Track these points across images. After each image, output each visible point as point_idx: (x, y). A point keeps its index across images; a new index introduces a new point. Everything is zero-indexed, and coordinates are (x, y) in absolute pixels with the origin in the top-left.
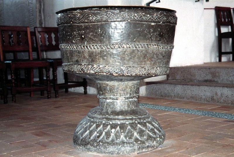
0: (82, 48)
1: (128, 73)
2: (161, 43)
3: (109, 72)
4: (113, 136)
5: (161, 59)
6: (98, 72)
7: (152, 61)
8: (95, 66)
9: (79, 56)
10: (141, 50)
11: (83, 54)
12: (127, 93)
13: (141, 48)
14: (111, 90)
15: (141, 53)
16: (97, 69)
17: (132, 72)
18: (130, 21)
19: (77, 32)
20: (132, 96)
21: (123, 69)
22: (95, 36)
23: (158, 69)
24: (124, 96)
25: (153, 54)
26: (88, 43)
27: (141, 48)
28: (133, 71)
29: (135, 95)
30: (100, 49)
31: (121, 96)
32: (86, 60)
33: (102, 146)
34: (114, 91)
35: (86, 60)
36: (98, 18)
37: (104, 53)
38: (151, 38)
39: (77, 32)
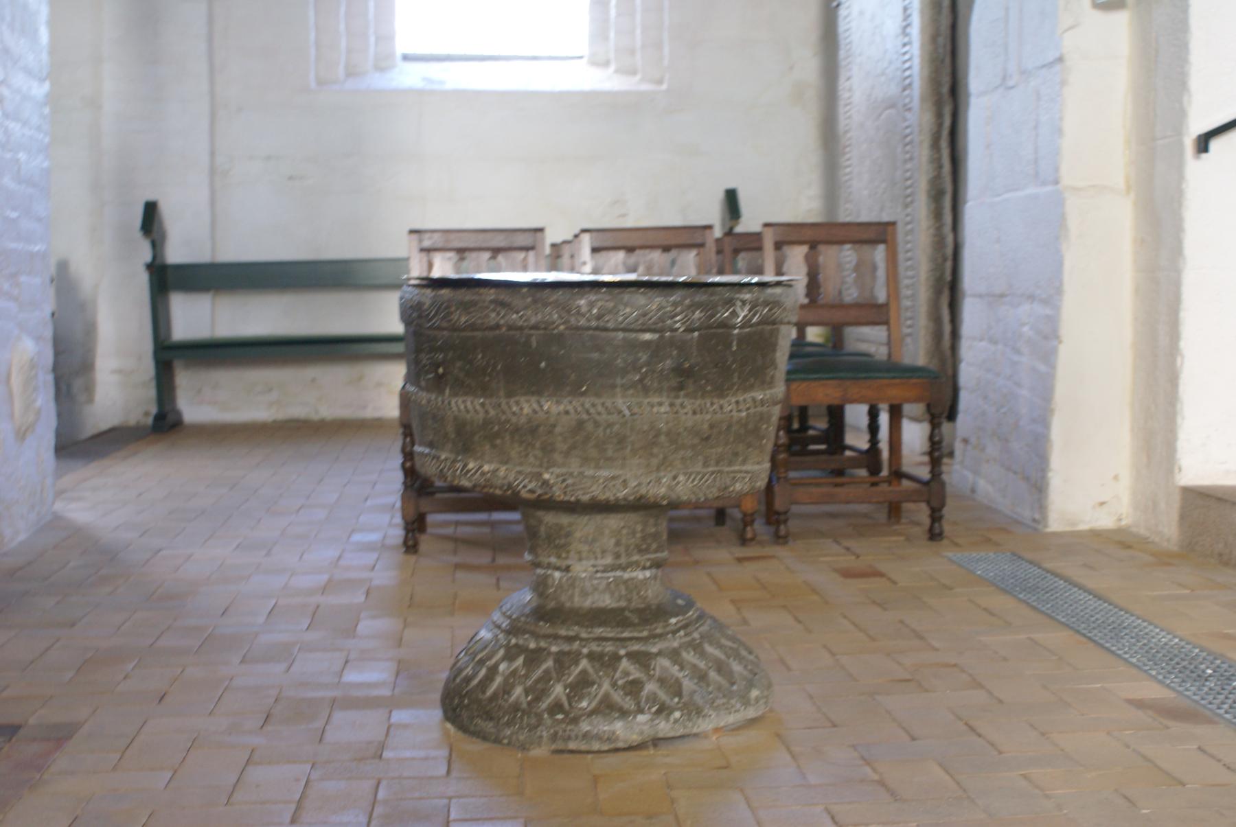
2: (686, 396)
8: (471, 466)
14: (549, 538)
20: (623, 560)
31: (580, 559)
32: (450, 445)
38: (641, 380)
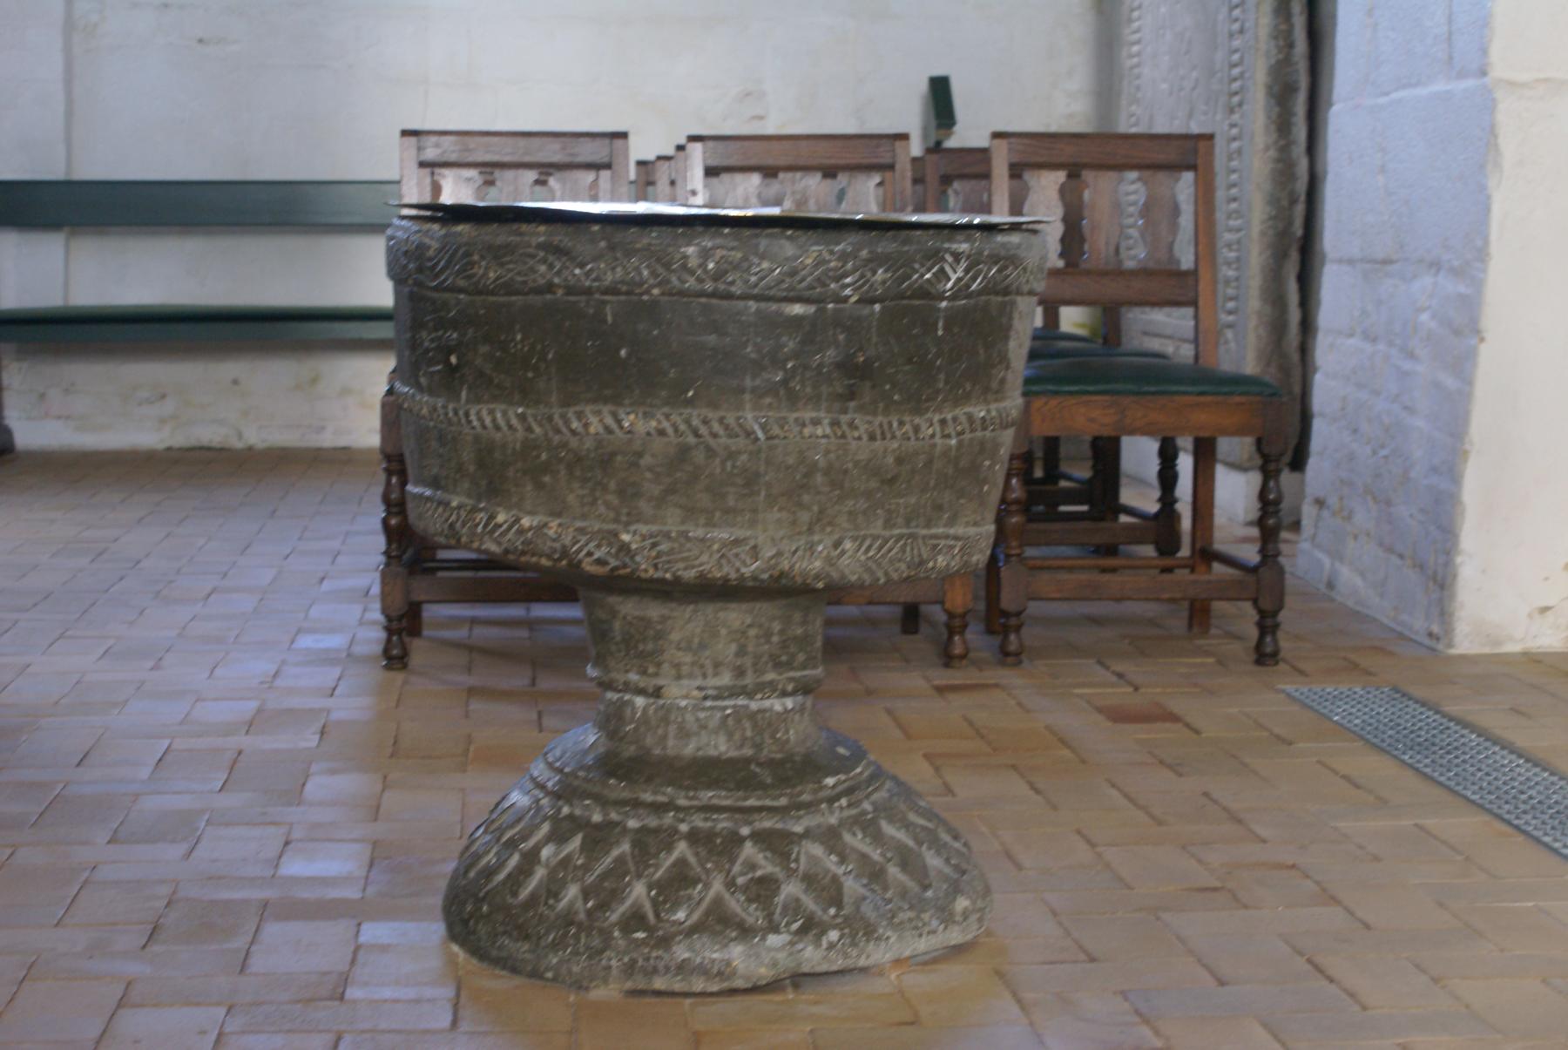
1: (656, 567)
3: (565, 552)
5: (868, 494)
7: (800, 505)
10: (727, 448)
12: (717, 665)
13: (723, 440)
15: (729, 464)
16: (510, 535)
17: (681, 565)
18: (663, 294)
20: (749, 680)
21: (634, 546)
23: (843, 552)
24: (699, 682)
25: (803, 469)
27: (723, 440)
28: (683, 559)
29: (770, 676)
30: (520, 434)
31: (679, 677)
34: (641, 647)
36: (510, 271)
37: (538, 456)
38: (785, 382)
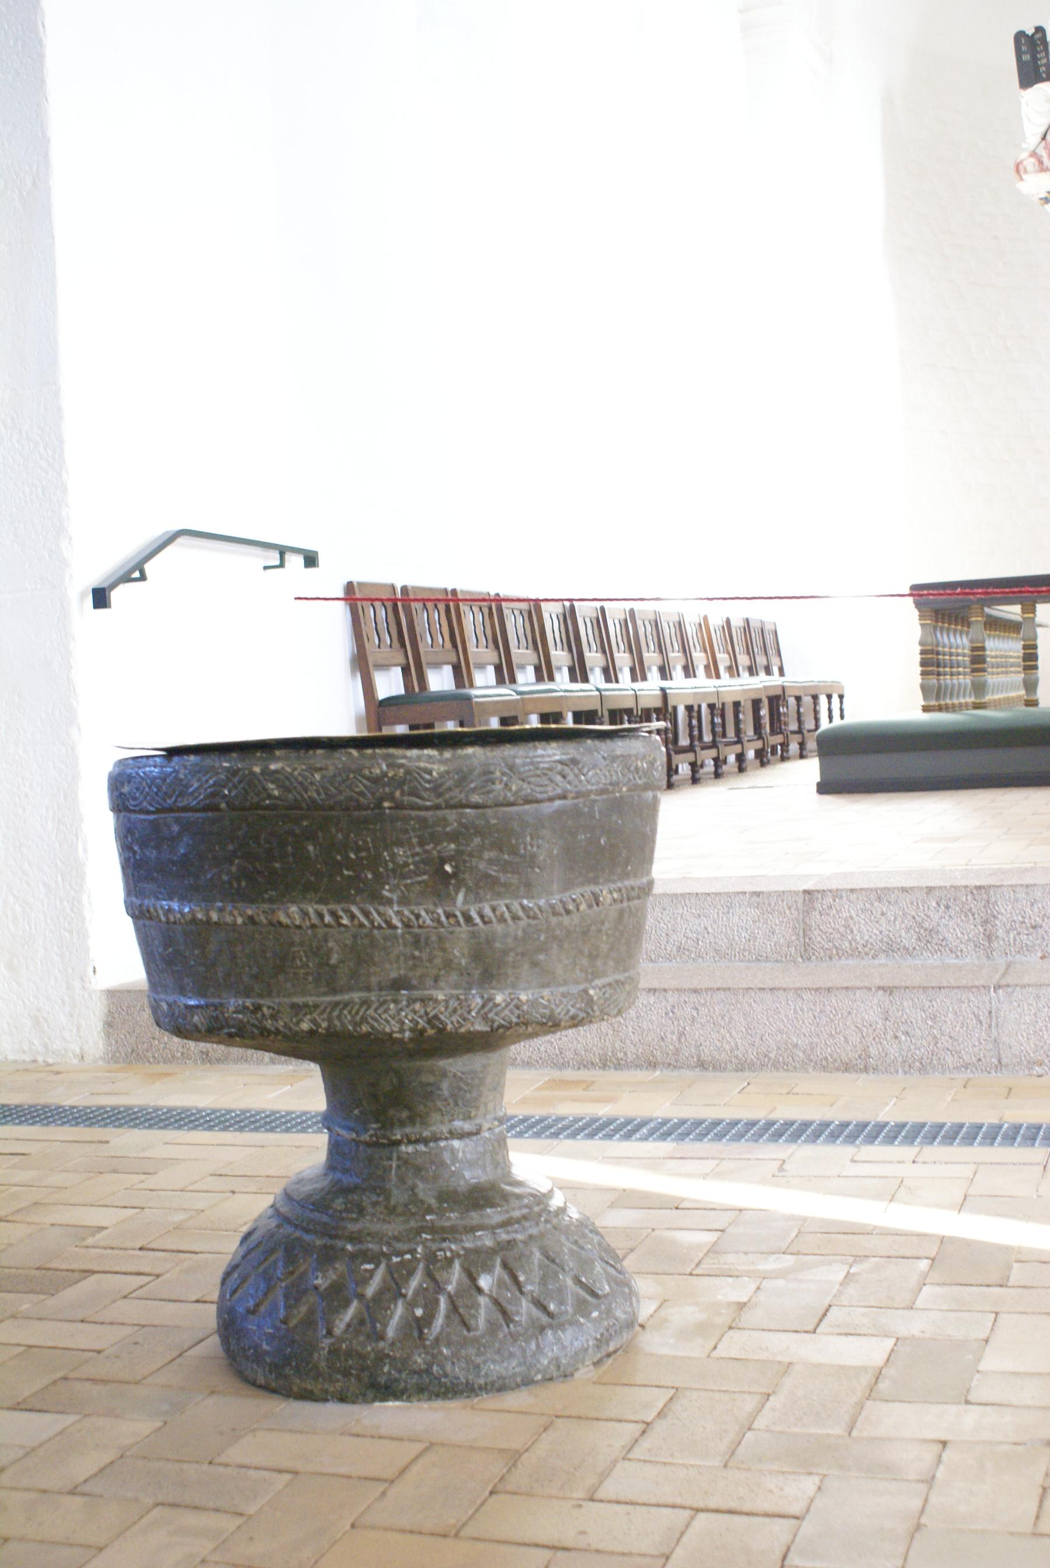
0: (439, 921)
4: (486, 1307)
6: (510, 1023)
9: (414, 957)
11: (444, 950)
16: (507, 1012)
19: (418, 849)
22: (505, 867)
26: (472, 896)
33: (453, 1363)
35: (454, 977)
39: (418, 849)
